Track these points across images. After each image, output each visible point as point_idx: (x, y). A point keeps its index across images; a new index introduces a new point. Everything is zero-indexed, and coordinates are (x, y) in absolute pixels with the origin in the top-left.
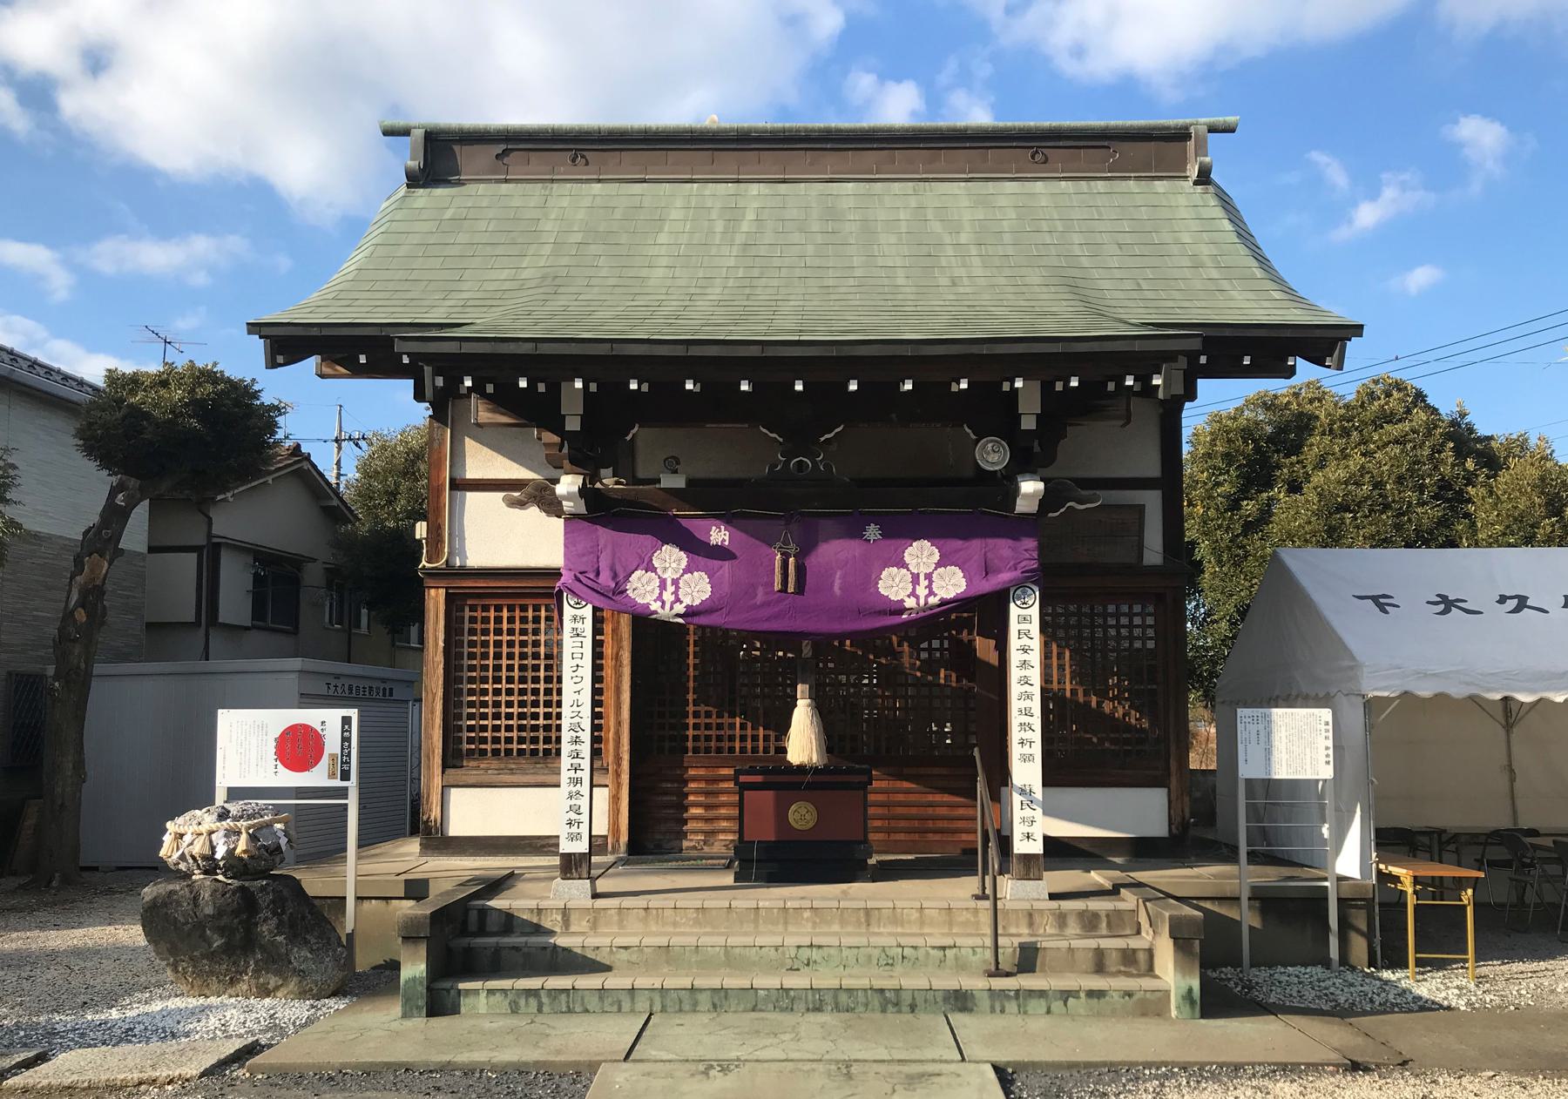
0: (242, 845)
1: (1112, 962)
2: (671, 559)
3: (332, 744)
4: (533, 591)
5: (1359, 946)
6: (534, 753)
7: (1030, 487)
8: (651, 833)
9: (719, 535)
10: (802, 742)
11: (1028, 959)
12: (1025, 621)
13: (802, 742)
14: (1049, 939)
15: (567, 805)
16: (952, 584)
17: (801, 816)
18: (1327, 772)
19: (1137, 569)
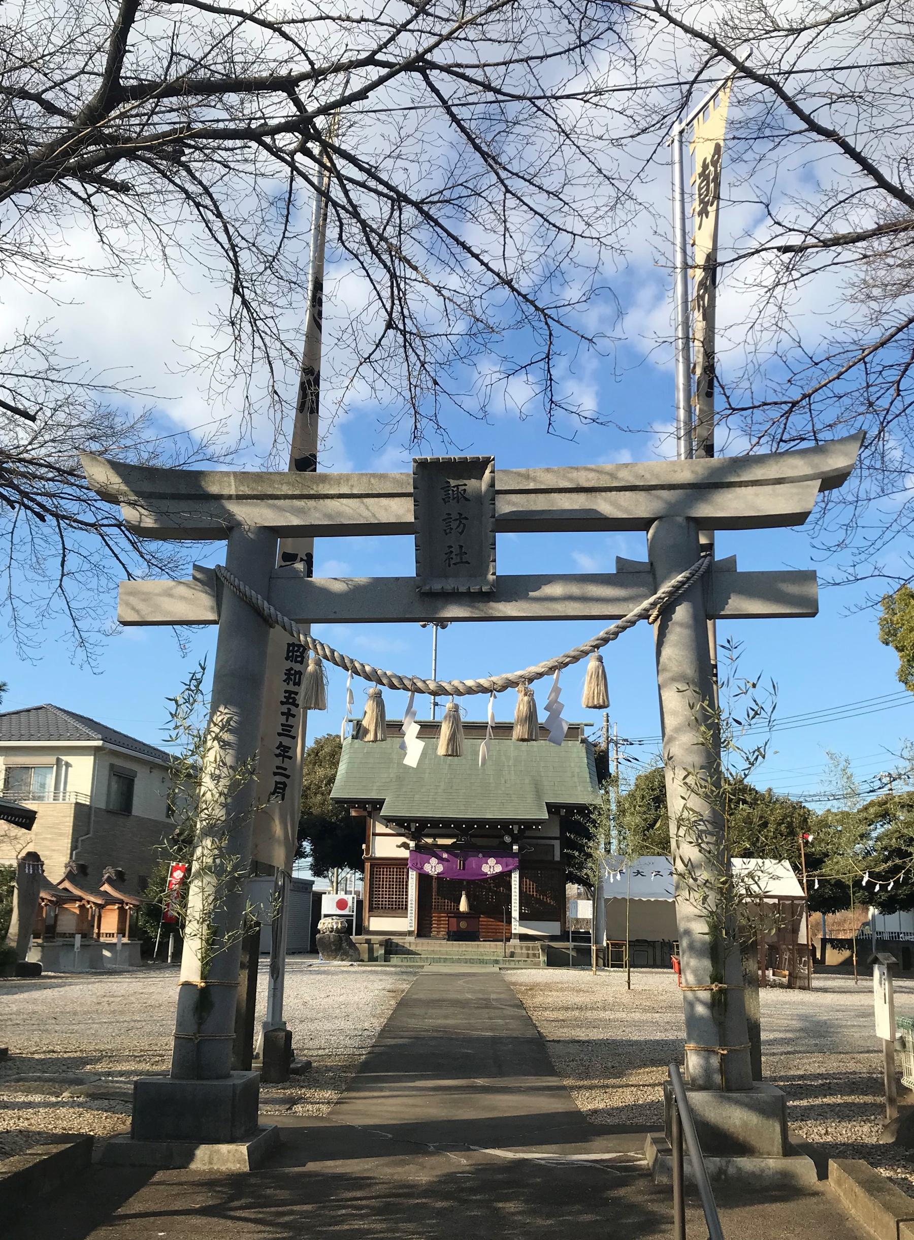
0: (340, 926)
1: (531, 955)
2: (434, 861)
3: (350, 904)
4: (399, 864)
5: (601, 961)
6: (399, 909)
7: (515, 847)
8: (423, 930)
9: (445, 856)
10: (463, 906)
11: (512, 955)
12: (515, 878)
13: (463, 906)
14: (518, 951)
15: (406, 923)
16: (499, 869)
17: (463, 925)
18: (591, 917)
19: (553, 862)
